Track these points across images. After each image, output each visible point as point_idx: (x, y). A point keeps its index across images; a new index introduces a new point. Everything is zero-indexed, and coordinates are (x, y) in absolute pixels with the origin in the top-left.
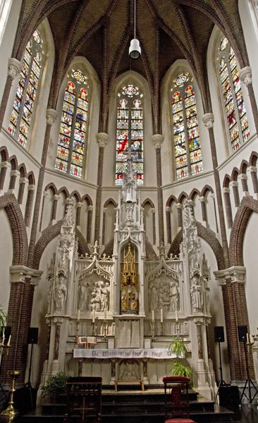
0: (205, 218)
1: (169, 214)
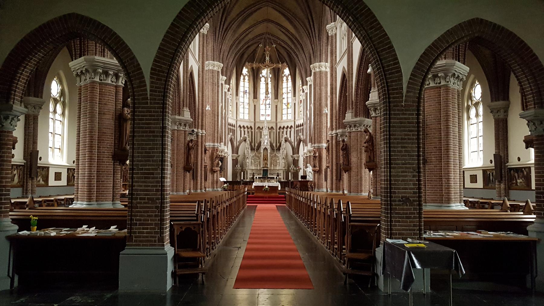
0: (290, 137)
1: (279, 133)
